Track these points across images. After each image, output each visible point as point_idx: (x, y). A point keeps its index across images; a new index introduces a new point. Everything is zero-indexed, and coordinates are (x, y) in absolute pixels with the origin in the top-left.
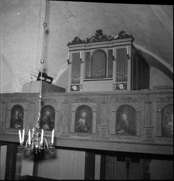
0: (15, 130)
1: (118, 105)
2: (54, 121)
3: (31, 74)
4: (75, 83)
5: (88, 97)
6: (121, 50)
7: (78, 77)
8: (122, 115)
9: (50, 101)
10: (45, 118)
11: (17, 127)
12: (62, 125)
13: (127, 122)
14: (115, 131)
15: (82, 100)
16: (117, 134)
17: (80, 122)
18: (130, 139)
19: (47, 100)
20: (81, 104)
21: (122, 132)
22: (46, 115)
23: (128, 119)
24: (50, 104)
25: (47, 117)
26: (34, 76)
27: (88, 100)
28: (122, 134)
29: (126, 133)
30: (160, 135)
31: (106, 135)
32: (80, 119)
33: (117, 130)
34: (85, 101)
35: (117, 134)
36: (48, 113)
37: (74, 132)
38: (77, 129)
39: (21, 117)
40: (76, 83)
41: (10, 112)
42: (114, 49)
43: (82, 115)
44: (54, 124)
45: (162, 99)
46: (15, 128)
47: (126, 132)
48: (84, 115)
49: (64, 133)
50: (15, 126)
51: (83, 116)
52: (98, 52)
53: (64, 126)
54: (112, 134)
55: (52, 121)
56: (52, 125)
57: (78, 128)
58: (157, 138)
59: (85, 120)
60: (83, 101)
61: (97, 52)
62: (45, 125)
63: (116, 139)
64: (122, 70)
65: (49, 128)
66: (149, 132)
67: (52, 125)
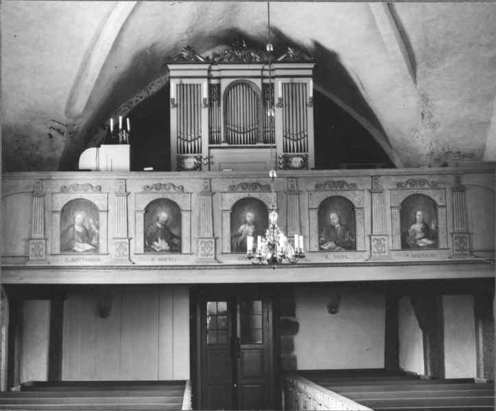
0: (76, 257)
1: (402, 196)
2: (181, 233)
3: (49, 126)
4: (294, 151)
5: (345, 179)
6: (288, 86)
7: (194, 140)
8: (329, 215)
9: (169, 189)
10: (157, 227)
11: (80, 250)
12: (200, 240)
13: (338, 228)
14: (317, 244)
15: (245, 186)
16: (321, 250)
17: (243, 231)
18: (432, 255)
19: (420, 182)
20: (329, 194)
21: (329, 245)
22: (158, 220)
23: (339, 222)
24: (169, 197)
25: (162, 225)
26: (59, 130)
27: (90, 188)
28: (330, 250)
29: (338, 248)
30: (400, 248)
31: (385, 252)
32: (241, 225)
33: (321, 243)
34: (251, 190)
35: (321, 250)
36: (163, 215)
37: (229, 251)
38: (235, 246)
39: (91, 228)
40: (297, 151)
41: (142, 215)
42: (279, 84)
43: (245, 218)
44: (180, 238)
45: (399, 185)
46: (156, 251)
47: (337, 245)
48: (249, 216)
49: (207, 255)
50: (76, 248)
51: (248, 219)
52: (238, 86)
53: (378, 237)
54: (312, 250)
55: (175, 232)
56: (176, 241)
57: (237, 243)
58: (393, 253)
59: (253, 227)
60: (415, 187)
61: (237, 85)
62: (157, 241)
63: (148, 260)
64: (242, 126)
65: (168, 248)
66: (381, 243)
67: (176, 241)
